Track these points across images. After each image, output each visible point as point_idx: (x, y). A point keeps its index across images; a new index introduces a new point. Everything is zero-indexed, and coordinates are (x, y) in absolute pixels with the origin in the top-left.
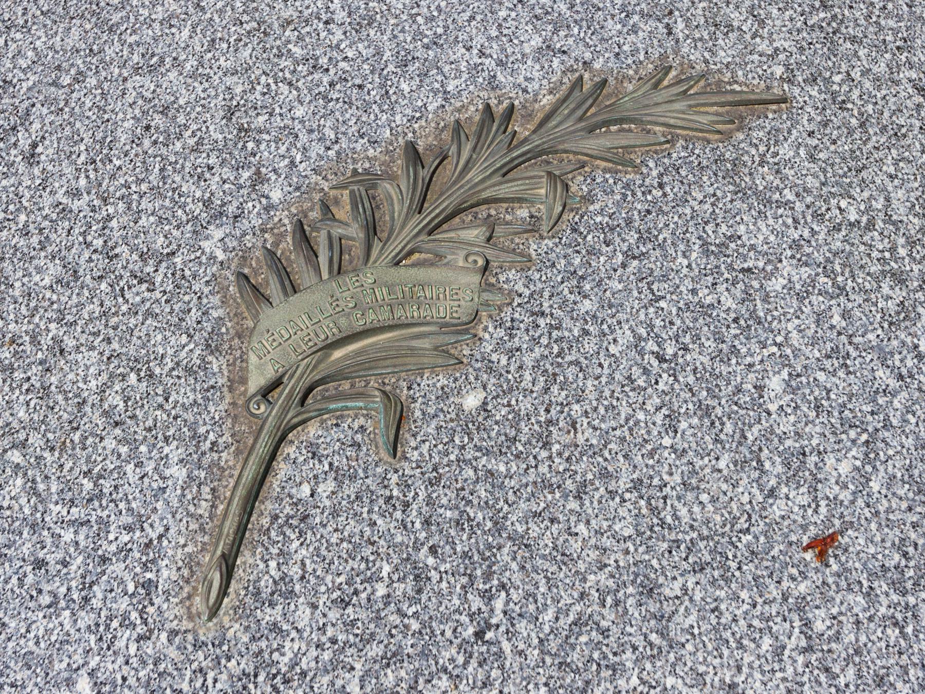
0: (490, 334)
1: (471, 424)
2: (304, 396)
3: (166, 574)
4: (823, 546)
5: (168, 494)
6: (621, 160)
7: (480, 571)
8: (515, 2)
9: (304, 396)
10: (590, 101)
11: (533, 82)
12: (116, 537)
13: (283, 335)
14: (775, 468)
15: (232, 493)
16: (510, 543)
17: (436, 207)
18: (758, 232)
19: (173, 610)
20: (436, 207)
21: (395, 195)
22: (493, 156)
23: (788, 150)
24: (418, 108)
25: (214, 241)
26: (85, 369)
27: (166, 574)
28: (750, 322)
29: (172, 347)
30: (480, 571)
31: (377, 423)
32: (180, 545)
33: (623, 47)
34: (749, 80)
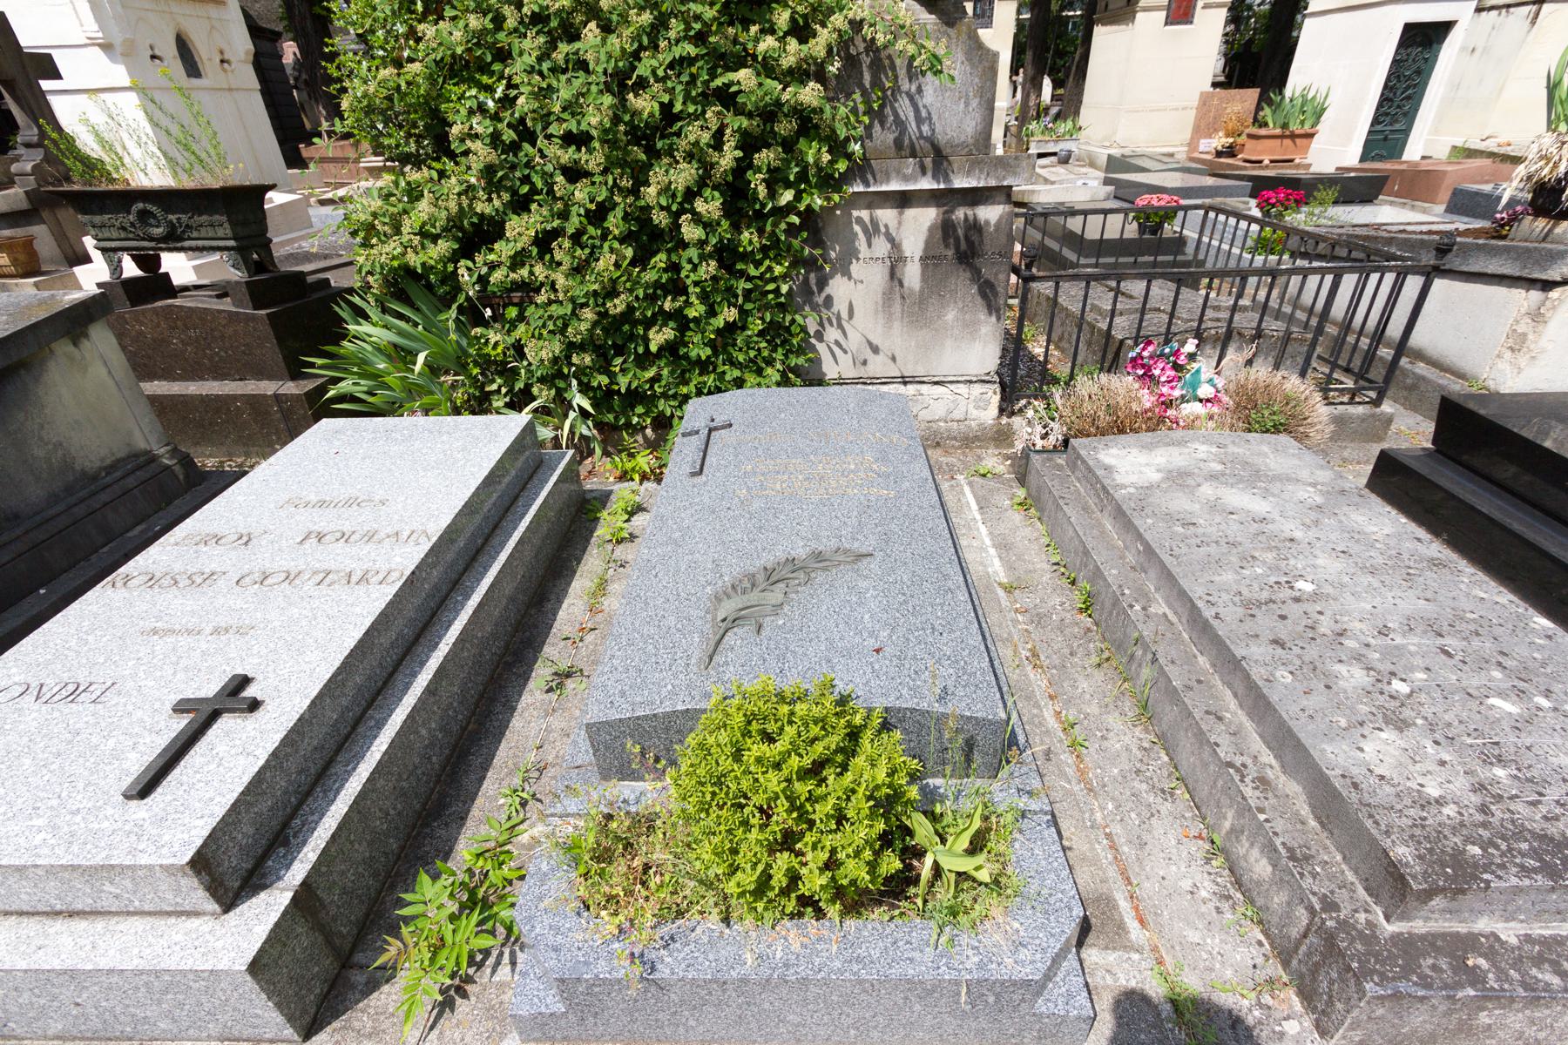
0: (786, 608)
1: (780, 627)
2: (734, 622)
3: (693, 661)
4: (877, 651)
5: (696, 646)
6: (825, 569)
7: (782, 658)
8: (271, 4)
9: (734, 622)
10: (818, 556)
11: (800, 552)
12: (679, 654)
13: (728, 608)
14: (865, 635)
15: (712, 643)
16: (815, 817)
17: (773, 579)
18: (863, 584)
19: (695, 669)
20: (773, 579)
21: (760, 578)
22: (790, 567)
23: (874, 565)
24: (768, 559)
25: (709, 589)
26: (672, 621)
27: (693, 661)
28: (860, 604)
29: (696, 613)
30: (782, 658)
31: (754, 628)
32: (697, 654)
33: (827, 545)
34: (864, 550)
